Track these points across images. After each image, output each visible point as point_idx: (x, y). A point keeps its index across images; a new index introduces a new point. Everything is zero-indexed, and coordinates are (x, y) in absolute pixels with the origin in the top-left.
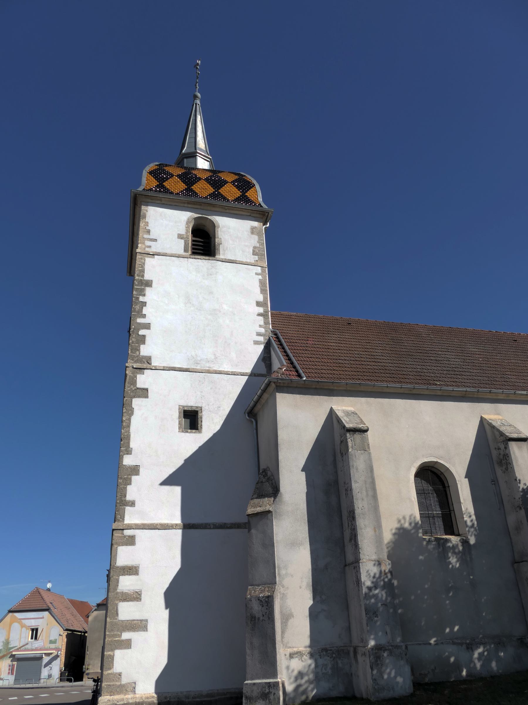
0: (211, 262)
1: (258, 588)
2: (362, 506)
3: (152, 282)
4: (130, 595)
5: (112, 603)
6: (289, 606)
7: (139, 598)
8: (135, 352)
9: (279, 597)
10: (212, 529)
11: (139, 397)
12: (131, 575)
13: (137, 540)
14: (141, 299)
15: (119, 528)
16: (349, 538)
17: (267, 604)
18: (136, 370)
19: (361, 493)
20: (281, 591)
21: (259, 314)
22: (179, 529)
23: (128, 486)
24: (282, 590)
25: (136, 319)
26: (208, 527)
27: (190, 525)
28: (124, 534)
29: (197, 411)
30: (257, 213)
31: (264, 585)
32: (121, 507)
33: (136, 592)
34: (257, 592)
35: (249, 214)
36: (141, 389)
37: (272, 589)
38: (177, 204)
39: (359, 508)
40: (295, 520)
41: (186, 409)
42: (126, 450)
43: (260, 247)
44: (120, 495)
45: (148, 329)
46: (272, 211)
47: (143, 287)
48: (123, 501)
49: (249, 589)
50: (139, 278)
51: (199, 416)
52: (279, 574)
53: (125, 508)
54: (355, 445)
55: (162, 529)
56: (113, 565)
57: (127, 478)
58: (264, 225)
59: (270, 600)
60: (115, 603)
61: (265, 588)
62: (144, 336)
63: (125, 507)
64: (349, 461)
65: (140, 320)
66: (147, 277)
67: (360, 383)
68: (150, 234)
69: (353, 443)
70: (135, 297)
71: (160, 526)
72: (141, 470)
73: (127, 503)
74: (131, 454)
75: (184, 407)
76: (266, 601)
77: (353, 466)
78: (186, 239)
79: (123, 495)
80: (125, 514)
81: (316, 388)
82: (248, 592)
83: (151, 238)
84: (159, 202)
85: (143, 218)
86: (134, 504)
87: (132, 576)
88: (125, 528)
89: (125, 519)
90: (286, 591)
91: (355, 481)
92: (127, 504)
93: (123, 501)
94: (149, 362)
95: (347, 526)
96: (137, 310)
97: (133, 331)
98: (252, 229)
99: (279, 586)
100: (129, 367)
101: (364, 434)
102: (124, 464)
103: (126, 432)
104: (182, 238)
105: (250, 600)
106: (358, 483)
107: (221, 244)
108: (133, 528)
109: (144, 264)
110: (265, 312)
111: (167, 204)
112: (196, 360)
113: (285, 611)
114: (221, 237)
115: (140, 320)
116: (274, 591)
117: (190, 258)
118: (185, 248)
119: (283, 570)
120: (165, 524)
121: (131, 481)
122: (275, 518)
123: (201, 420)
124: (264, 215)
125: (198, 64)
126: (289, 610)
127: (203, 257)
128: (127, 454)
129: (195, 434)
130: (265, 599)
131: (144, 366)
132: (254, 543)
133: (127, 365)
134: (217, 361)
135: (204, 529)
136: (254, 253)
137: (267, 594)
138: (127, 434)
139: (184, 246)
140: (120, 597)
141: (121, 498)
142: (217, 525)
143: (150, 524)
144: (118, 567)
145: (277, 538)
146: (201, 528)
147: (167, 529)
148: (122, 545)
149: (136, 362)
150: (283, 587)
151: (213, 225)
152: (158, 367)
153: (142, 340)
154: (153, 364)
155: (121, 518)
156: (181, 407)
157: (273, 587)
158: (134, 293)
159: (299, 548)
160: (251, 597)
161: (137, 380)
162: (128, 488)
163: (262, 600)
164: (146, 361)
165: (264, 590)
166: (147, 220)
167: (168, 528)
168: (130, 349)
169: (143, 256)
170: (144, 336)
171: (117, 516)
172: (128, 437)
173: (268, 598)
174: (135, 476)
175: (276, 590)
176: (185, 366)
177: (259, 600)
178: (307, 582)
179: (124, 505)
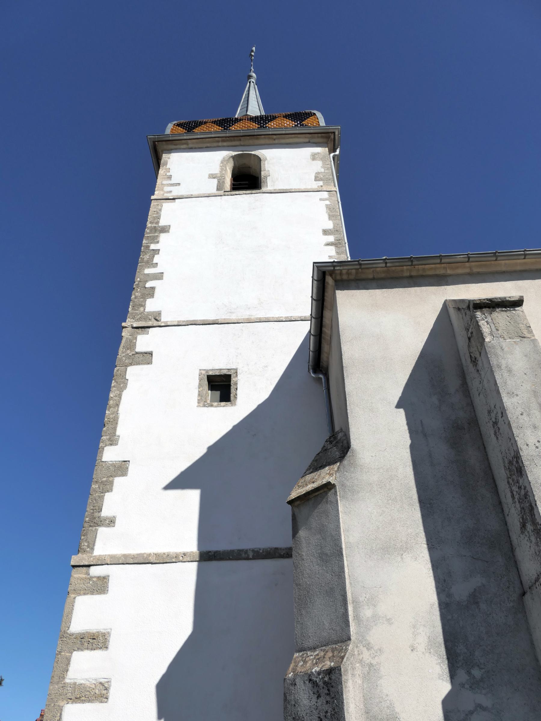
0: (254, 195)
1: (312, 653)
2: (536, 441)
3: (170, 227)
4: (88, 689)
5: (52, 705)
6: (387, 695)
7: (105, 696)
8: (139, 308)
9: (358, 672)
10: (251, 559)
11: (138, 364)
12: (94, 649)
13: (112, 585)
14: (153, 247)
15: (82, 564)
16: (519, 524)
17: (329, 690)
18: (138, 330)
19: (529, 415)
20: (364, 659)
21: (328, 243)
22: (189, 562)
23: (107, 494)
24: (366, 655)
25: (144, 269)
26: (243, 555)
27: (210, 554)
28: (89, 574)
29: (230, 376)
30: (318, 137)
31: (325, 646)
32: (91, 528)
33: (101, 683)
34: (309, 664)
35: (307, 140)
36: (142, 353)
37: (339, 652)
38: (208, 145)
39: (530, 444)
40: (388, 500)
41: (211, 373)
42: (109, 439)
43: (326, 171)
44: (92, 509)
45: (159, 280)
46: (339, 128)
47: (156, 234)
48: (95, 518)
49: (295, 659)
50: (152, 225)
51: (232, 382)
52: (357, 617)
53: (96, 531)
54: (497, 330)
55: (158, 562)
56: (64, 631)
57: (106, 481)
58: (330, 152)
59: (333, 678)
60: (59, 706)
61: (327, 652)
62: (153, 289)
63: (97, 528)
64: (488, 358)
65: (147, 271)
66: (163, 222)
67: (495, 253)
68: (171, 180)
69: (493, 327)
70: (144, 246)
71: (154, 558)
72: (131, 468)
73: (101, 521)
74: (117, 444)
75: (207, 371)
76: (325, 683)
77: (499, 367)
78: (221, 177)
79: (97, 508)
80: (97, 539)
81: (411, 277)
82: (292, 666)
83: (173, 183)
84: (184, 146)
85: (164, 165)
86: (114, 523)
87: (95, 651)
88: (92, 563)
89: (96, 547)
90: (376, 658)
91: (508, 393)
92: (102, 522)
93: (95, 518)
94: (157, 318)
95: (510, 500)
96: (145, 259)
97: (138, 284)
98: (313, 155)
99: (357, 647)
100: (126, 327)
101: (515, 310)
102: (103, 460)
103: (113, 414)
104: (214, 178)
105: (292, 684)
106: (517, 395)
107: (269, 176)
108: (106, 562)
109: (160, 210)
110: (338, 240)
111: (195, 148)
112: (230, 309)
113: (377, 708)
114: (269, 169)
115: (147, 271)
116: (343, 658)
117: (225, 195)
118: (218, 187)
119: (366, 607)
120: (164, 554)
121: (112, 486)
122: (343, 497)
123: (235, 387)
124: (328, 138)
125: (252, 51)
126: (388, 707)
127: (243, 191)
128: (111, 445)
129: (225, 407)
130: (323, 678)
131: (149, 324)
132: (304, 557)
133: (124, 324)
134: (263, 307)
135: (236, 561)
136: (317, 179)
137: (328, 664)
138: (114, 415)
139: (217, 185)
140: (70, 694)
141: (93, 513)
142: (261, 551)
143: (137, 555)
144: (73, 634)
145: (348, 537)
146: (230, 559)
147: (166, 563)
148: (84, 594)
149: (138, 320)
150: (368, 649)
151: (259, 160)
152: (170, 322)
153: (151, 292)
154: (162, 320)
155: (88, 546)
156: (203, 372)
157: (342, 649)
158: (144, 241)
159: (402, 558)
160: (296, 675)
161: (137, 342)
162: (105, 497)
163: (316, 681)
164: (153, 318)
165: (324, 657)
166: (168, 167)
167: (168, 561)
168: (130, 306)
169: (160, 202)
170: (153, 289)
171: (82, 544)
172: (115, 421)
173: (329, 675)
174: (120, 478)
175: (347, 653)
176: (211, 317)
177: (310, 680)
178: (428, 634)
179: (96, 525)
